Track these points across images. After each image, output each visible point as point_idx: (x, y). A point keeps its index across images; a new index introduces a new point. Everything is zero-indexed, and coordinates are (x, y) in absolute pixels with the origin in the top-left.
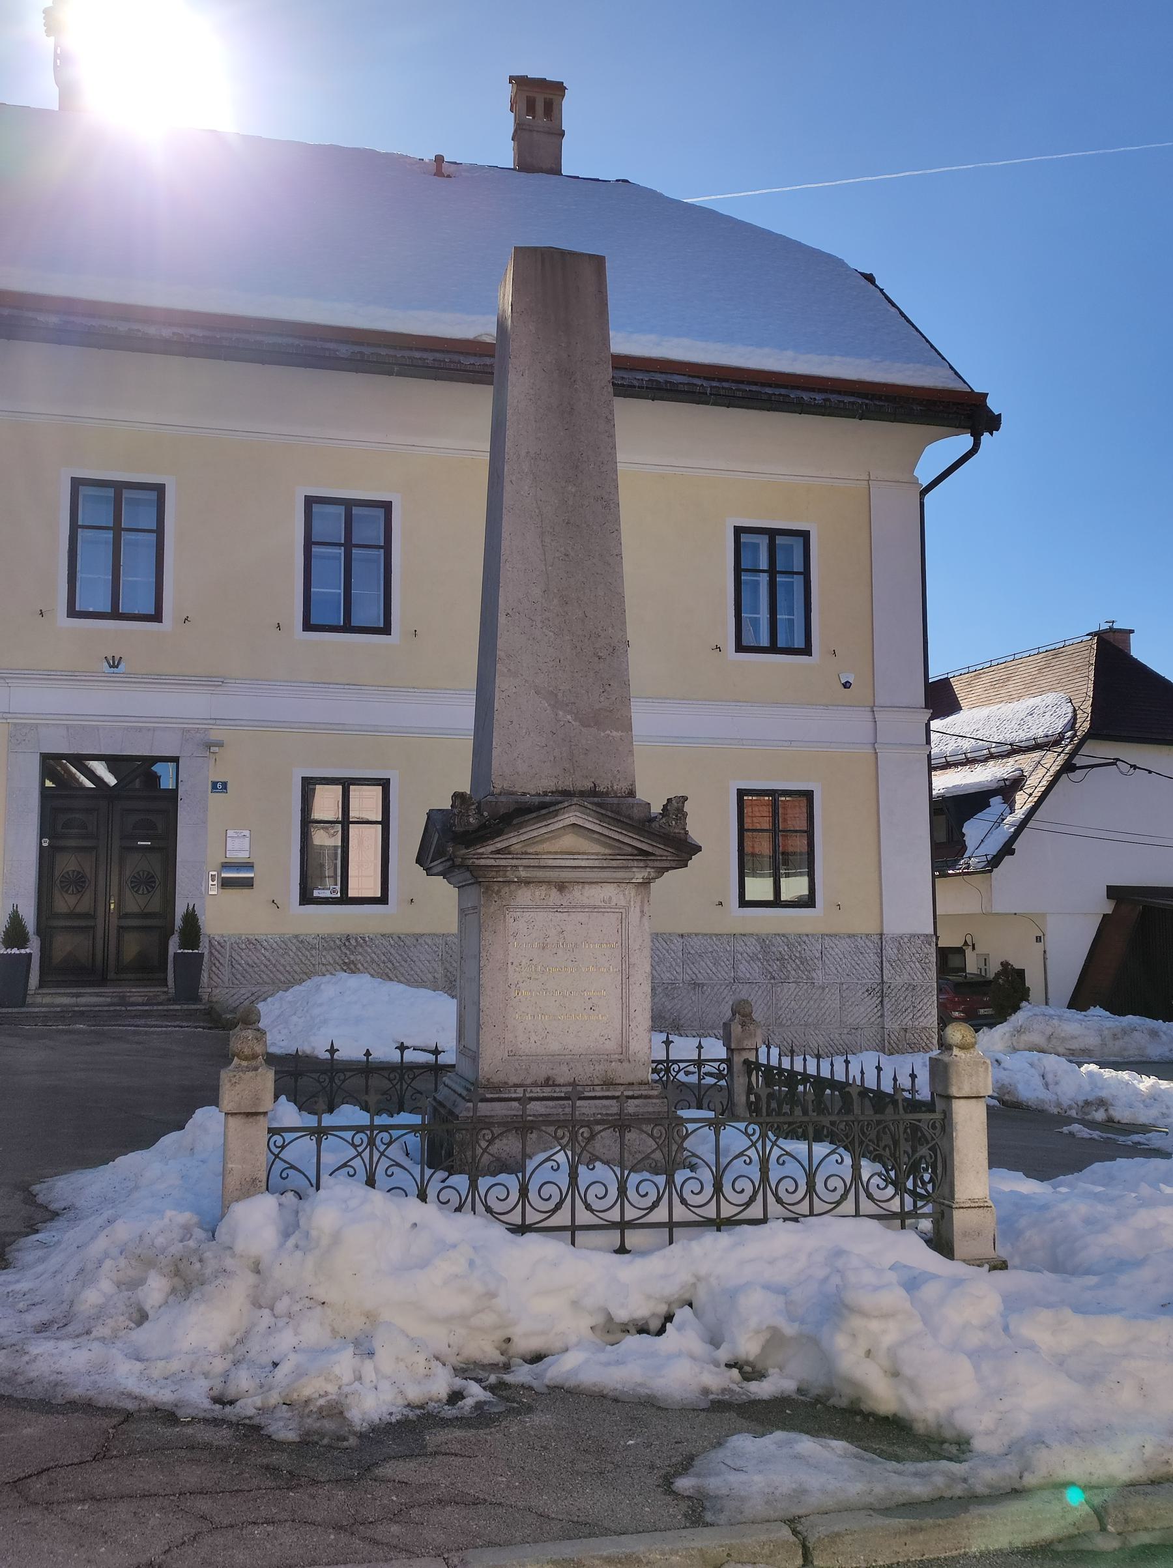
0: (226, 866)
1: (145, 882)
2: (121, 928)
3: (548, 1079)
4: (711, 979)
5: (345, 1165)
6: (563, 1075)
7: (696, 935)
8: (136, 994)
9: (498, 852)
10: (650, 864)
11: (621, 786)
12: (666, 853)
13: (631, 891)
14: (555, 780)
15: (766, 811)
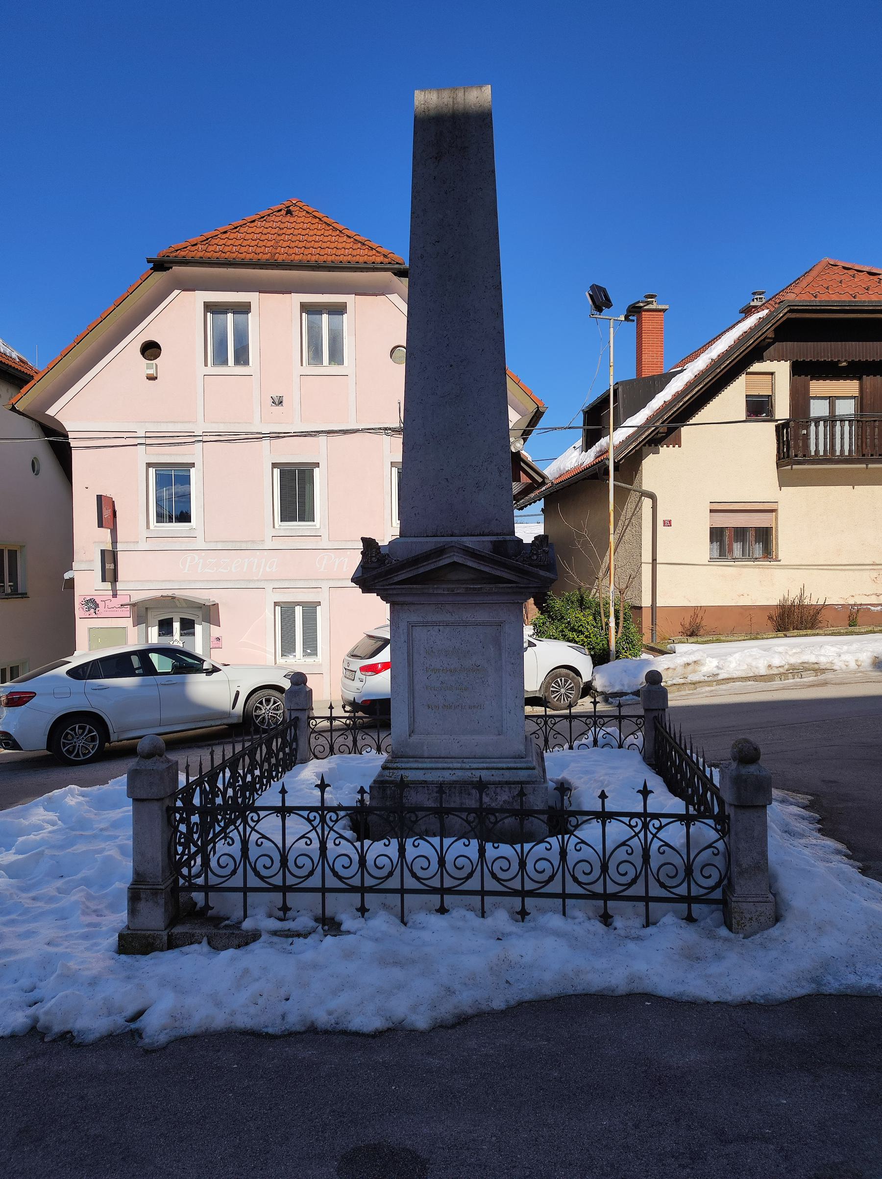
5: (303, 837)
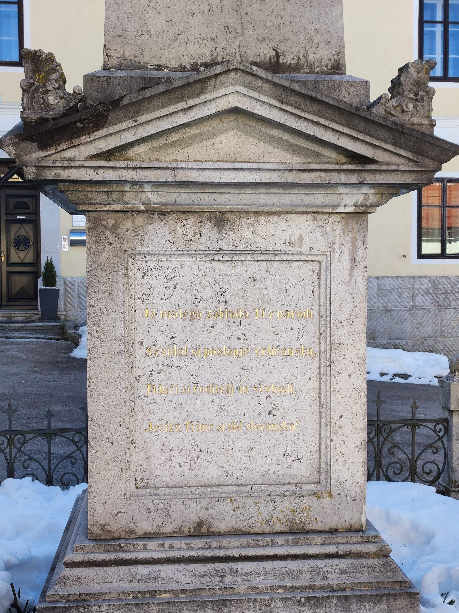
0: (73, 232)
1: (22, 243)
2: (9, 273)
3: (200, 524)
4: (397, 306)
6: (224, 517)
7: (388, 277)
8: (19, 315)
9: (108, 155)
10: (369, 178)
11: (321, 55)
12: (396, 159)
13: (335, 227)
14: (212, 46)
15: (438, 193)
